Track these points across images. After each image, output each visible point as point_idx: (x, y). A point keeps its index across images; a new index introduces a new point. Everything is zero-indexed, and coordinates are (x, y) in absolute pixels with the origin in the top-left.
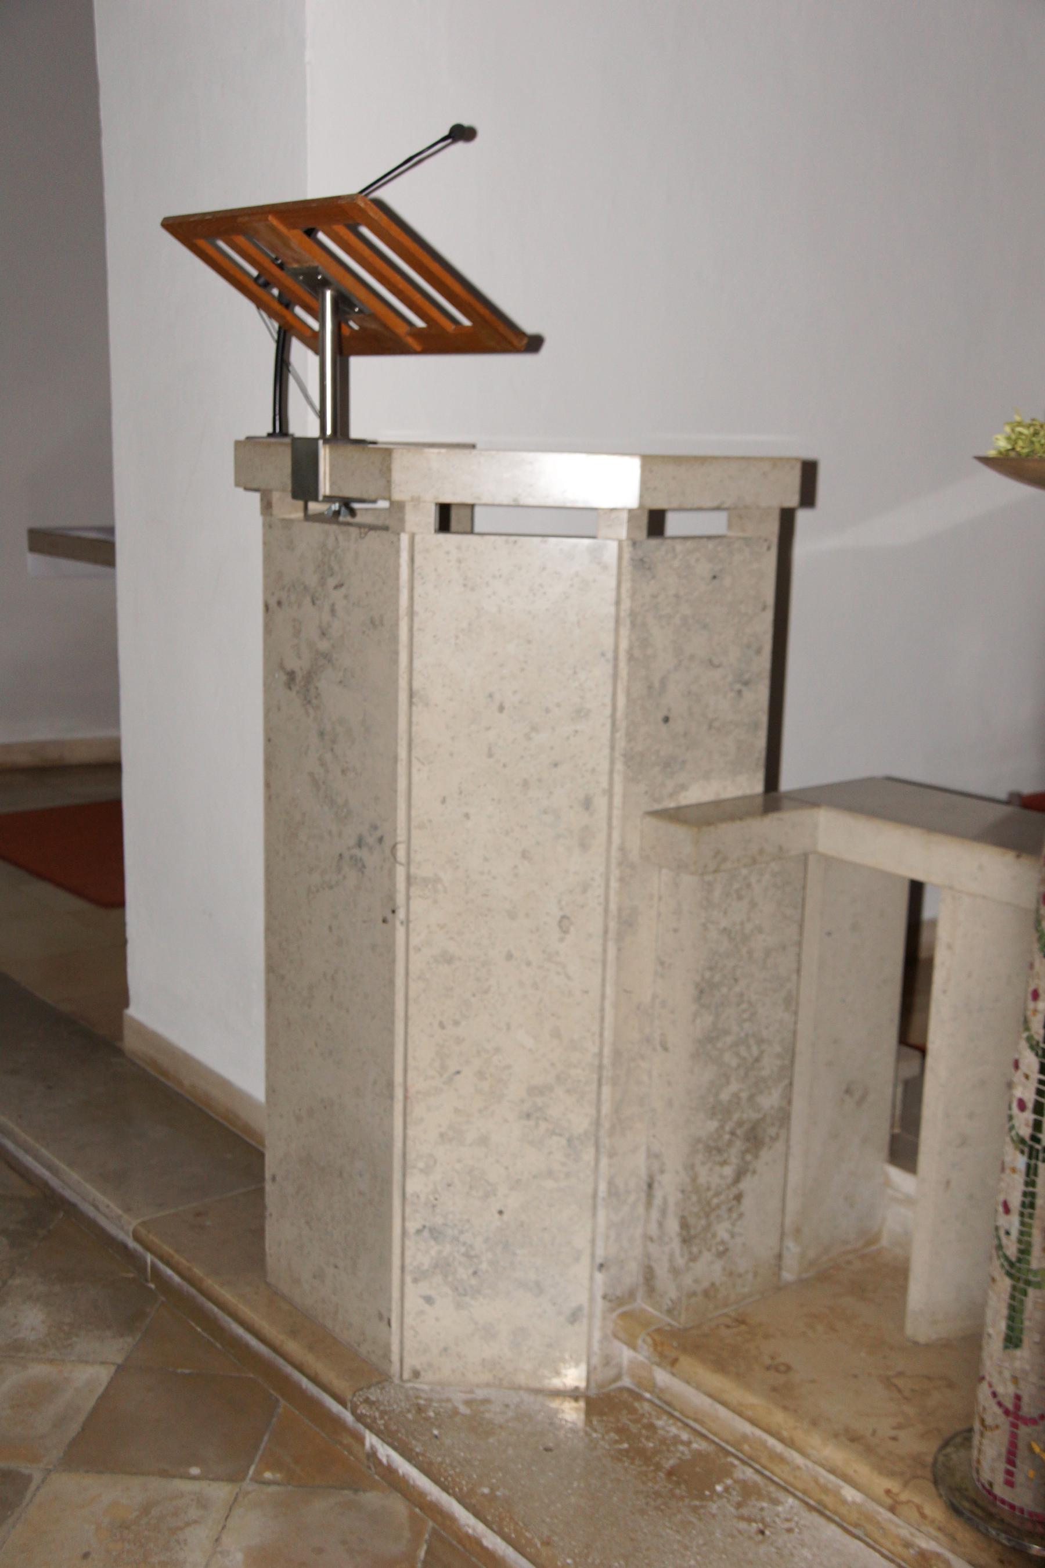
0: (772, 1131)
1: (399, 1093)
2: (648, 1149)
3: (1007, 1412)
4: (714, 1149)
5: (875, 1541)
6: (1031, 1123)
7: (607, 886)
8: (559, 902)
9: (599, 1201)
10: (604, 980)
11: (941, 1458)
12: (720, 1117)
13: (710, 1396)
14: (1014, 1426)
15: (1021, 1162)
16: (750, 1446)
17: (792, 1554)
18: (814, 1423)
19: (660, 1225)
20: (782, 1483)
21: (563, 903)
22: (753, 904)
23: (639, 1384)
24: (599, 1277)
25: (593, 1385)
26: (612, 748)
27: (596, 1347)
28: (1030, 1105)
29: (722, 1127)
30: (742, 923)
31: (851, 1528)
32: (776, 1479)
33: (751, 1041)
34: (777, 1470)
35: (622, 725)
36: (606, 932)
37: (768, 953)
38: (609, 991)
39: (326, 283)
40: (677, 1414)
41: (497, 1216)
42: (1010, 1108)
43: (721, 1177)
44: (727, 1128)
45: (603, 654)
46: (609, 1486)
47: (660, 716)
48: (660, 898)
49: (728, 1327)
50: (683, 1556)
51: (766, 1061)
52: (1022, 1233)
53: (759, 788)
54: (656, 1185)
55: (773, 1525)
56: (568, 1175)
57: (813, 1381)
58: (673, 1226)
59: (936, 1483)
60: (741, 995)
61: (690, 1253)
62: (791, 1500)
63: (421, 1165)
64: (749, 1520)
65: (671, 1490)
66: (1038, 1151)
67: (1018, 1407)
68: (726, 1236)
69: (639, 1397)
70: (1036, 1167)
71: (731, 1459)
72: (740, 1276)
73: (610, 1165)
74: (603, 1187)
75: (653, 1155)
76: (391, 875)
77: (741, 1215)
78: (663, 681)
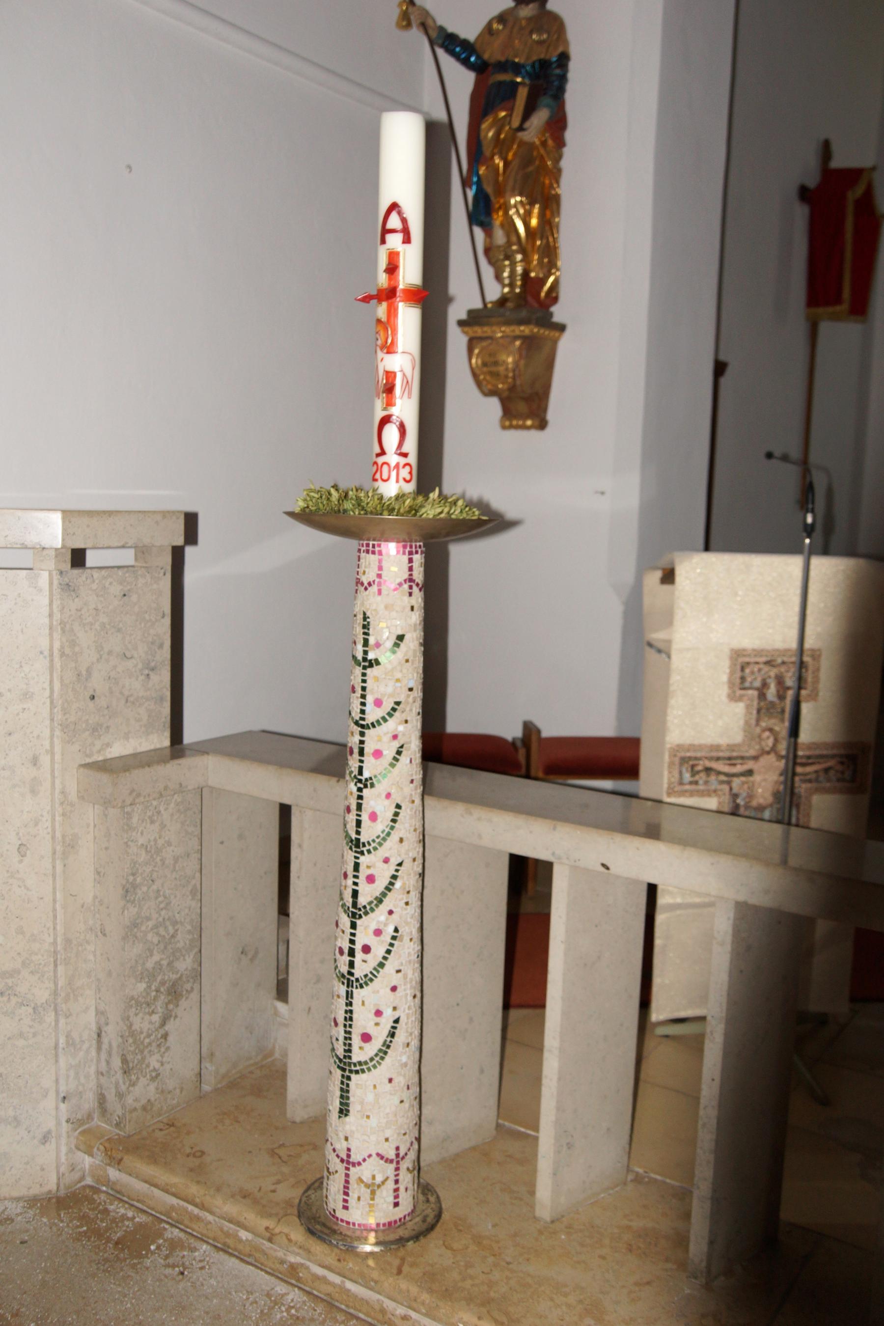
3: (342, 1161)
4: (144, 1004)
5: (262, 1264)
6: (347, 963)
8: (18, 834)
10: (54, 889)
11: (304, 1199)
12: (147, 980)
13: (146, 1182)
14: (347, 1169)
15: (342, 990)
16: (176, 1213)
17: (202, 1285)
18: (218, 1189)
19: (108, 1063)
20: (199, 1236)
21: (21, 834)
22: (163, 826)
23: (98, 1181)
24: (63, 1106)
26: (52, 720)
27: (63, 1159)
28: (346, 951)
29: (149, 987)
30: (155, 840)
31: (246, 1258)
32: (195, 1233)
33: (168, 923)
34: (195, 1227)
36: (54, 853)
37: (176, 860)
40: (125, 1199)
42: (335, 955)
43: (151, 1023)
44: (153, 987)
46: (69, 1261)
47: (88, 695)
48: (95, 826)
49: (161, 1130)
50: (122, 1302)
51: (179, 936)
52: (346, 1038)
53: (167, 743)
54: (103, 1033)
55: (190, 1266)
56: (35, 1035)
58: (117, 1062)
59: (299, 1217)
60: (158, 891)
61: (130, 1081)
62: (205, 1246)
64: (173, 1266)
65: (117, 1255)
66: (352, 981)
67: (349, 1156)
69: (96, 1190)
70: (352, 991)
72: (170, 1092)
74: (62, 1041)
75: (99, 1013)
77: (168, 1048)
78: (89, 671)
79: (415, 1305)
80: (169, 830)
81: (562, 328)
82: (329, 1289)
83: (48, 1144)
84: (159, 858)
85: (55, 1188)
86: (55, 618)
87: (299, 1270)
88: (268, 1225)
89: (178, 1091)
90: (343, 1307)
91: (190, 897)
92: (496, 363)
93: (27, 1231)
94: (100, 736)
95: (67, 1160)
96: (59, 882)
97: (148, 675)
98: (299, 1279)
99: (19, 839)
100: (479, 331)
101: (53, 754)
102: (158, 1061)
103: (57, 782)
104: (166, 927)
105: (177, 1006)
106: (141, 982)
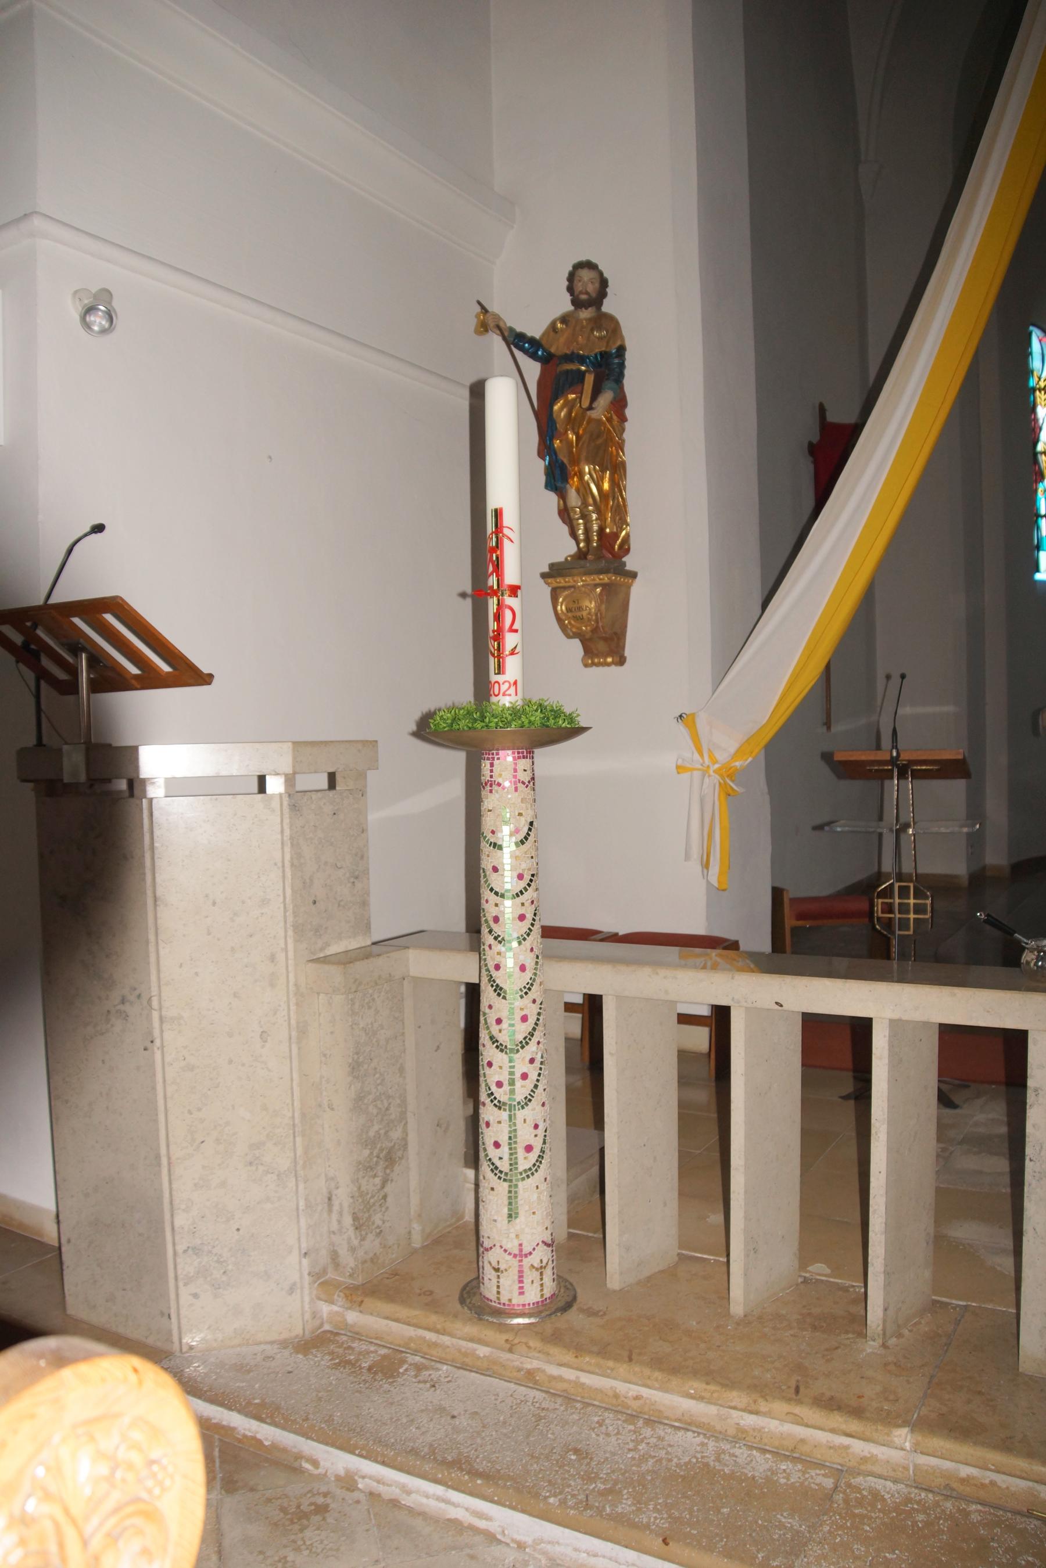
0: (399, 1154)
1: (164, 1161)
2: (326, 1175)
7: (289, 1009)
9: (300, 1212)
19: (339, 1222)
22: (377, 1012)
24: (305, 1262)
25: (307, 1332)
26: (285, 922)
27: (307, 1307)
29: (372, 1153)
30: (372, 1024)
31: (483, 1372)
33: (383, 1097)
34: (434, 1352)
35: (290, 907)
38: (295, 1076)
39: (83, 649)
41: (236, 1232)
43: (374, 1185)
44: (375, 1154)
45: (276, 864)
49: (388, 1278)
54: (334, 1197)
57: (448, 1296)
58: (348, 1220)
60: (375, 1069)
62: (445, 1367)
63: (183, 1207)
64: (425, 1382)
68: (380, 1223)
71: (403, 1355)
73: (305, 1188)
74: (302, 1203)
75: (329, 1179)
76: (149, 1018)
79: (649, 1382)
80: (381, 1015)
81: (634, 575)
82: (565, 1386)
83: (294, 1294)
84: (375, 1040)
85: (301, 1332)
86: (285, 834)
87: (536, 1374)
88: (507, 1338)
89: (396, 1246)
90: (579, 1398)
91: (398, 1075)
92: (580, 609)
93: (289, 1365)
94: (321, 935)
95: (310, 1308)
96: (295, 1063)
97: (354, 882)
98: (536, 1382)
99: (261, 1027)
100: (561, 581)
101: (287, 952)
102: (380, 1219)
103: (291, 976)
104: (382, 1101)
105: (393, 1171)
106: (365, 1149)
